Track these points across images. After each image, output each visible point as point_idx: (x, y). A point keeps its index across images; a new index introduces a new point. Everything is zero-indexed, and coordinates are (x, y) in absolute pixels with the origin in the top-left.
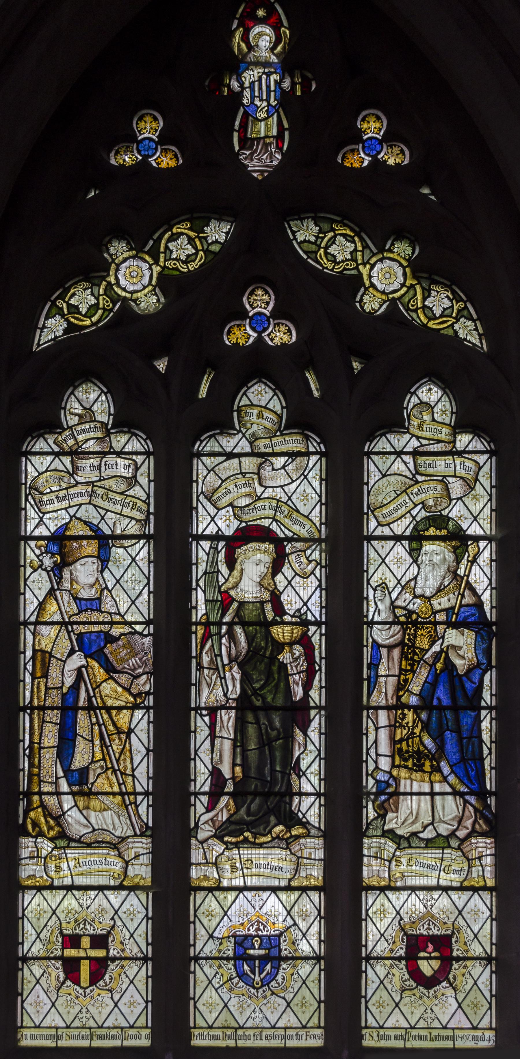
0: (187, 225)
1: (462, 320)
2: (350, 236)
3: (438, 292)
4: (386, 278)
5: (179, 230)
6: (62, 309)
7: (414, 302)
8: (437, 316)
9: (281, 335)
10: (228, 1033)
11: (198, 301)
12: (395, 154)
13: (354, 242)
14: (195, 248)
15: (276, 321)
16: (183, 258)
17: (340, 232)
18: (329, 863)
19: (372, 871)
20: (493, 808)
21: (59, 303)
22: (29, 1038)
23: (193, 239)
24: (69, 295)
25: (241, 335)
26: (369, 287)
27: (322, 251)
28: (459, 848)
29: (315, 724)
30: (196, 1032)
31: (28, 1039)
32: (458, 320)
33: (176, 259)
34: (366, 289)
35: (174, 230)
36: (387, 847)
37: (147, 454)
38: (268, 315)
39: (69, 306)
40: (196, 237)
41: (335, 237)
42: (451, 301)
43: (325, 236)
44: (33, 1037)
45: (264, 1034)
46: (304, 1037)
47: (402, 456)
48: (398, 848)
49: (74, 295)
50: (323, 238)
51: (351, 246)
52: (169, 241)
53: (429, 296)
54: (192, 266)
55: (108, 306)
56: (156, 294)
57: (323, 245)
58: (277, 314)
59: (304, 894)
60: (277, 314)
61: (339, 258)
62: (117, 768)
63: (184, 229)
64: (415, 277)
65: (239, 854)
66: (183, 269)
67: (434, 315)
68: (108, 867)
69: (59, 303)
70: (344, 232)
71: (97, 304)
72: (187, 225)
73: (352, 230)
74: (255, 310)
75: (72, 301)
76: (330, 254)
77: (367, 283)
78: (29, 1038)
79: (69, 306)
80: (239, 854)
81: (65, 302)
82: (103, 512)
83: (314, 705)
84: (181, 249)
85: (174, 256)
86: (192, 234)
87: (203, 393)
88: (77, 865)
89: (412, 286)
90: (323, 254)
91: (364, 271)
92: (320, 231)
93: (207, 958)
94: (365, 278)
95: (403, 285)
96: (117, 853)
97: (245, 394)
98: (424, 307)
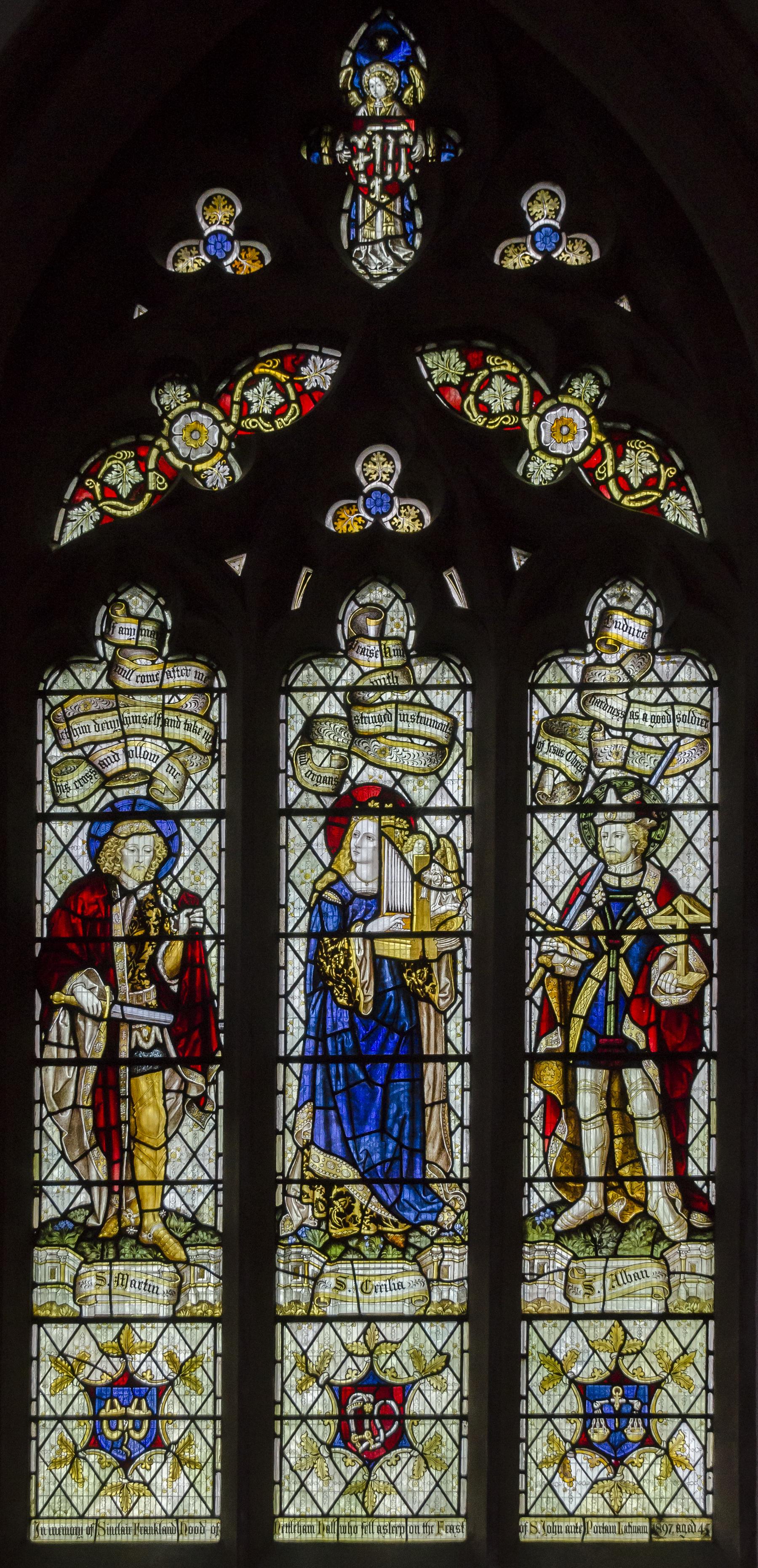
0: (274, 363)
1: (673, 494)
2: (510, 373)
3: (636, 451)
4: (561, 434)
5: (262, 370)
6: (93, 491)
7: (602, 470)
8: (636, 486)
9: (407, 519)
10: (326, 1523)
11: (293, 471)
12: (577, 252)
13: (519, 384)
14: (285, 395)
15: (404, 502)
16: (267, 410)
17: (497, 369)
18: (473, 1280)
19: (288, 1293)
20: (713, 1200)
21: (89, 482)
22: (47, 1532)
23: (283, 385)
24: (102, 471)
25: (347, 520)
26: (536, 450)
27: (471, 398)
28: (415, 1259)
29: (702, 1076)
30: (282, 1522)
31: (44, 1532)
32: (665, 494)
33: (256, 415)
34: (532, 453)
35: (257, 371)
36: (312, 1259)
37: (463, 687)
38: (392, 492)
39: (104, 485)
40: (288, 381)
41: (491, 375)
42: (658, 464)
43: (476, 376)
44: (53, 1531)
45: (376, 1524)
46: (435, 1530)
47: (672, 689)
48: (86, 1261)
49: (110, 469)
50: (472, 379)
51: (512, 391)
52: (246, 387)
53: (624, 458)
54: (281, 423)
55: (163, 486)
56: (228, 464)
57: (473, 388)
58: (403, 490)
59: (573, 1324)
60: (403, 490)
61: (496, 408)
62: (406, 1142)
63: (271, 368)
64: (602, 430)
65: (353, 1269)
66: (266, 427)
67: (631, 486)
68: (625, 1287)
69: (89, 482)
70: (503, 368)
71: (145, 483)
72: (274, 363)
73: (518, 365)
74: (374, 485)
75: (110, 479)
76: (482, 402)
77: (534, 444)
78: (47, 1532)
79: (104, 485)
80: (353, 1269)
81: (96, 480)
82: (398, 775)
83: (454, 1053)
84: (263, 398)
85: (254, 410)
86: (282, 377)
87: (459, 600)
88: (615, 1284)
89: (599, 444)
90: (472, 404)
91: (530, 425)
92: (468, 369)
93: (319, 1417)
94: (532, 435)
95: (587, 443)
96: (416, 1267)
97: (601, 596)
98: (617, 475)
